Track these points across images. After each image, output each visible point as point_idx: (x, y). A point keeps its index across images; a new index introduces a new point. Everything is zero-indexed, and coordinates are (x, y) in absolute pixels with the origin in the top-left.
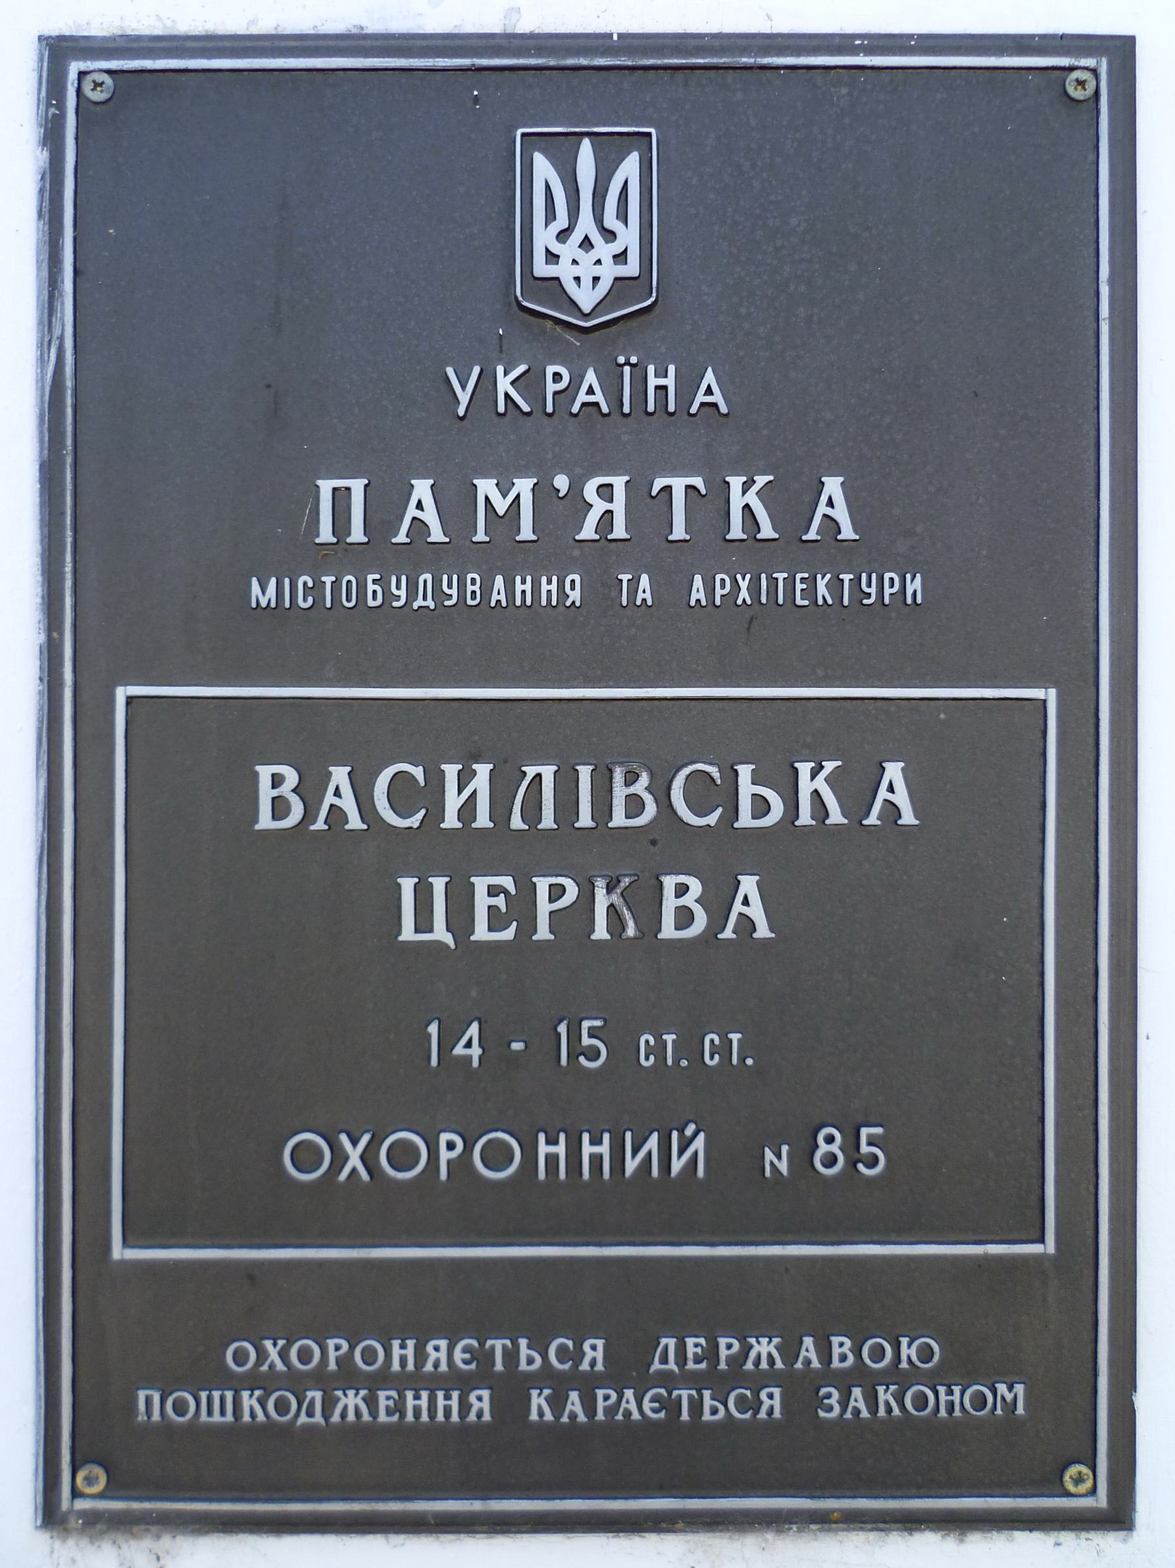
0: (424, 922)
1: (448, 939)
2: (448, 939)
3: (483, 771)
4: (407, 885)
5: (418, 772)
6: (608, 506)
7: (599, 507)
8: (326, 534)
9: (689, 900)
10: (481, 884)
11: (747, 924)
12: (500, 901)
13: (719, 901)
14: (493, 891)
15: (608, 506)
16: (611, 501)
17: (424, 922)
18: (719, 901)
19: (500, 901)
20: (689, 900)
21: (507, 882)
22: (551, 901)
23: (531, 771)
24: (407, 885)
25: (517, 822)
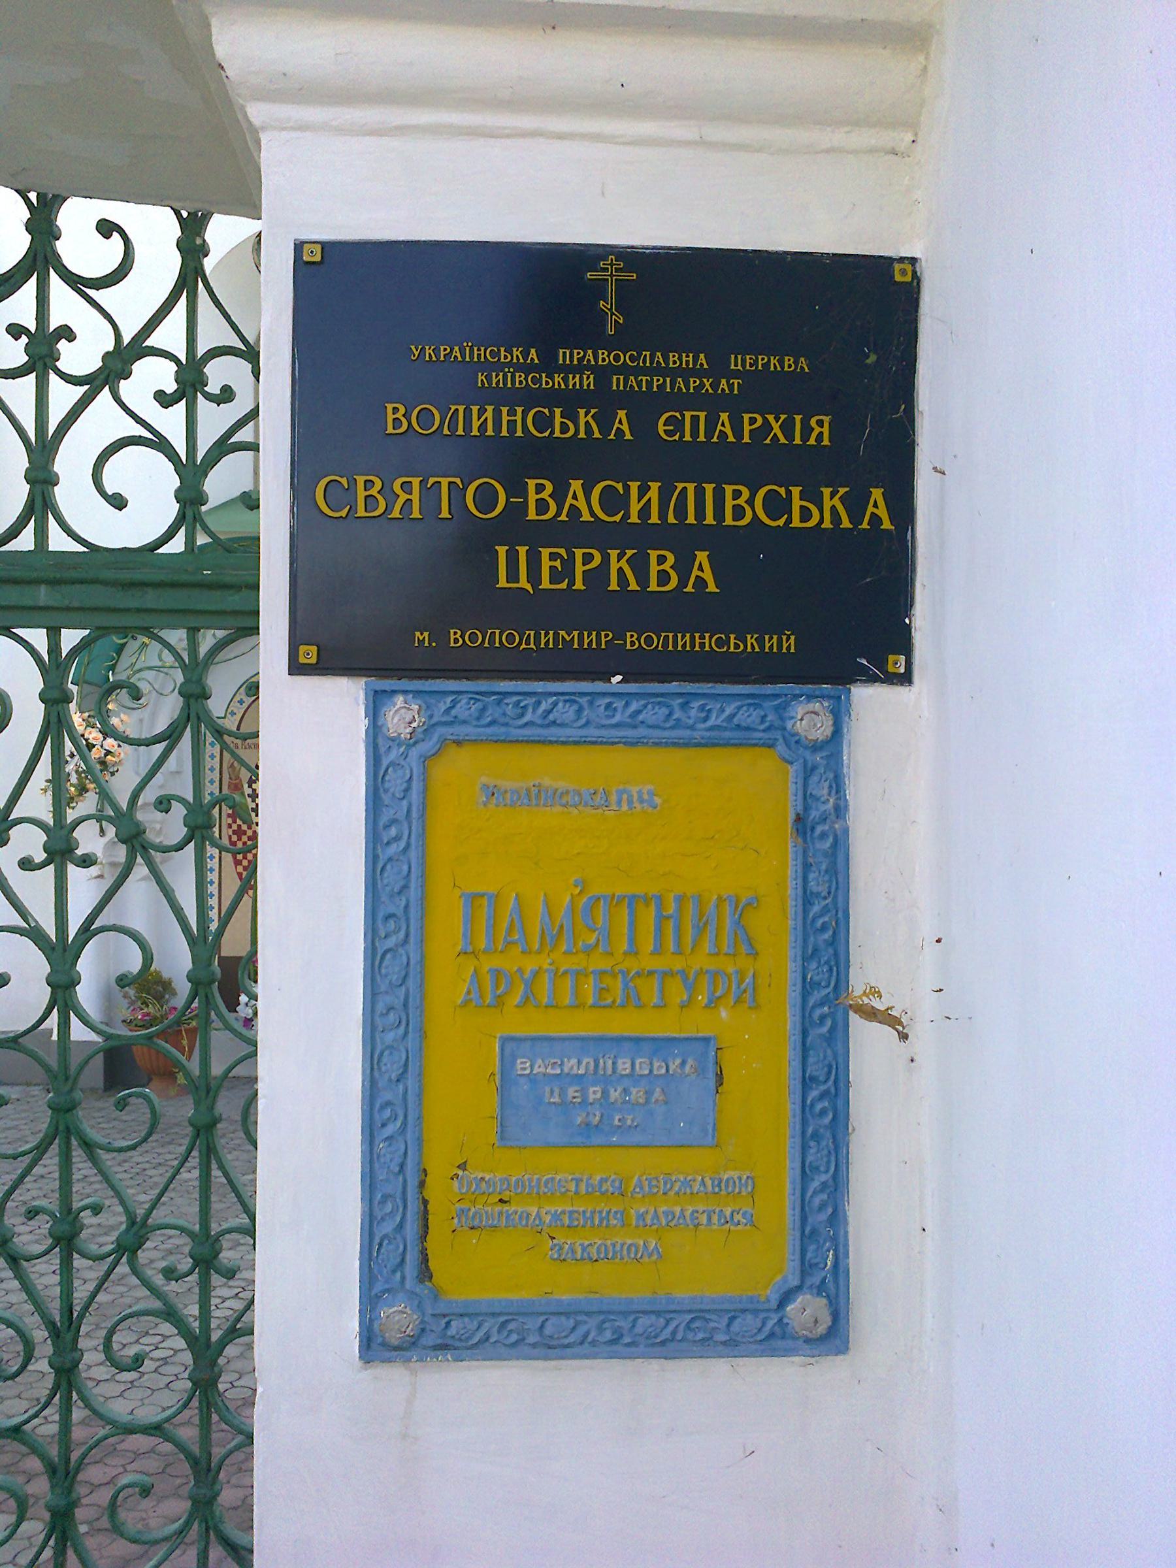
0: (513, 576)
1: (529, 587)
2: (529, 587)
3: (655, 486)
4: (502, 551)
5: (619, 487)
6: (409, 497)
7: (403, 497)
8: (615, 388)
9: (666, 566)
10: (545, 552)
11: (701, 582)
12: (558, 564)
13: (684, 566)
14: (553, 557)
15: (409, 497)
16: (411, 494)
17: (513, 576)
18: (684, 566)
19: (558, 564)
20: (666, 566)
21: (562, 551)
22: (584, 565)
23: (680, 486)
24: (502, 551)
25: (671, 519)
